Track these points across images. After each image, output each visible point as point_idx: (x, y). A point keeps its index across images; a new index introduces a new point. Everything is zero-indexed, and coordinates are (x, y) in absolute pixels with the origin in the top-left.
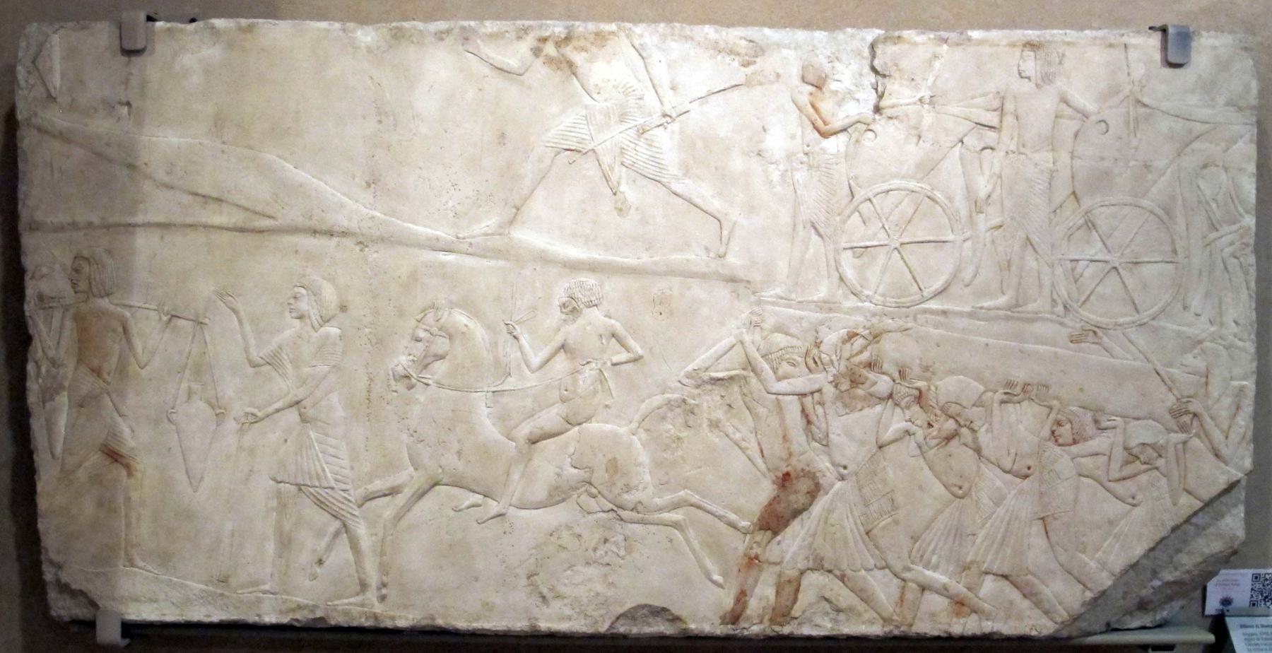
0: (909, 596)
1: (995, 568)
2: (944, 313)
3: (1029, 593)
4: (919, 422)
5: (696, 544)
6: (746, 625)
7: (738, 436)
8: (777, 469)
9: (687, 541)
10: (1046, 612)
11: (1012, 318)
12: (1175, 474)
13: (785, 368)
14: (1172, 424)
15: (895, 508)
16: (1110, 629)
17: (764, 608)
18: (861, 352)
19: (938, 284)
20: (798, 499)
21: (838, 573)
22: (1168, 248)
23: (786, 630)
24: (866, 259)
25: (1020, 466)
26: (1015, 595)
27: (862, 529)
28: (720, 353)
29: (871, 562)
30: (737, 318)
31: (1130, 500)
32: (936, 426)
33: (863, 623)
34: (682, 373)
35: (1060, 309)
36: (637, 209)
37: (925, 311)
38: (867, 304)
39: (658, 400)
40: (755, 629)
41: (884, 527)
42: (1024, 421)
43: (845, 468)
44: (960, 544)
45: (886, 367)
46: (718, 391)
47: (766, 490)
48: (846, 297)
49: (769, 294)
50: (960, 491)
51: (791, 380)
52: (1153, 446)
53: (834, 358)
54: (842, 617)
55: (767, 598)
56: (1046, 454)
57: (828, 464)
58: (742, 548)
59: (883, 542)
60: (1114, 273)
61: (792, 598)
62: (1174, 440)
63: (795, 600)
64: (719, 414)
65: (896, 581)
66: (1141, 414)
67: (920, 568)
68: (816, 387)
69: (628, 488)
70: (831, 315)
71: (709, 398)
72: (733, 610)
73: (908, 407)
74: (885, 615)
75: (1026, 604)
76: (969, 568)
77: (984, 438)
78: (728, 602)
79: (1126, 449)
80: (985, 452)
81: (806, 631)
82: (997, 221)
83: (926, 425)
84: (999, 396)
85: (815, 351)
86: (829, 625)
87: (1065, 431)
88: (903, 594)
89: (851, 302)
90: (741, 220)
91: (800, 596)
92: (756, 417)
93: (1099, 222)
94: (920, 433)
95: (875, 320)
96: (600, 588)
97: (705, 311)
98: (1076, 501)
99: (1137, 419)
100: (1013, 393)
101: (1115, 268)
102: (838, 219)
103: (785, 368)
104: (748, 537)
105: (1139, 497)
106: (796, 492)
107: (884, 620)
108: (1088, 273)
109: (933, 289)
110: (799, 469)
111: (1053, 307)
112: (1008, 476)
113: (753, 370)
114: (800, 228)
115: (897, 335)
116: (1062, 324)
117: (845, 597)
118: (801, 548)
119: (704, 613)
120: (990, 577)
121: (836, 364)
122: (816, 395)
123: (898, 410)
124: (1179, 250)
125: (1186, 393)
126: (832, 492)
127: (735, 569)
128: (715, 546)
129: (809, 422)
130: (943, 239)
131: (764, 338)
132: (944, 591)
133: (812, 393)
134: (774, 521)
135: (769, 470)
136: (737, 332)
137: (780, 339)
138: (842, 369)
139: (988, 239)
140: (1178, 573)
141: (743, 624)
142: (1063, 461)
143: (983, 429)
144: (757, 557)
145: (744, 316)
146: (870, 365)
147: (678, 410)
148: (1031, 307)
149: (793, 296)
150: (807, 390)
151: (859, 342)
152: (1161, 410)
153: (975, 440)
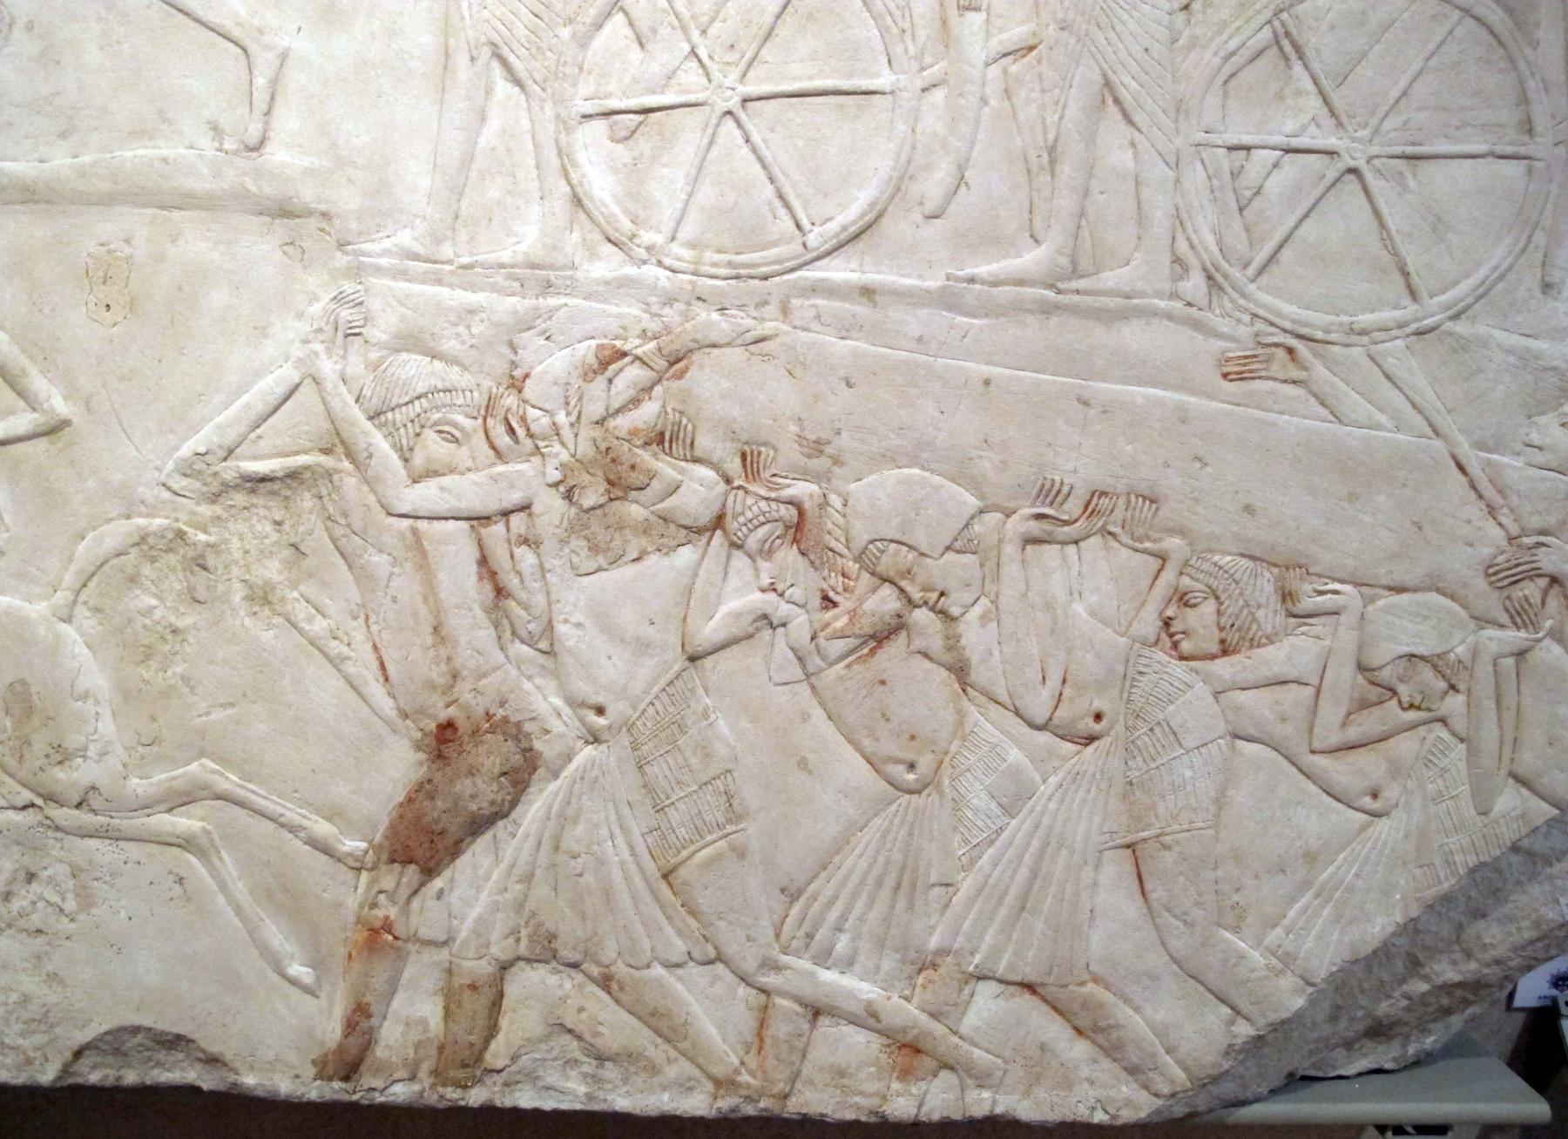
0: (779, 1029)
1: (1001, 969)
2: (868, 293)
3: (1091, 1026)
4: (796, 593)
5: (240, 888)
6: (378, 1083)
7: (319, 626)
8: (422, 712)
9: (224, 887)
10: (1132, 1071)
11: (1058, 308)
12: (1489, 735)
13: (433, 447)
14: (1492, 603)
15: (735, 816)
16: (1298, 1081)
17: (418, 1046)
18: (635, 402)
19: (850, 213)
20: (481, 791)
21: (595, 971)
22: (1508, 115)
23: (475, 1097)
24: (643, 144)
25: (1074, 711)
26: (1055, 1031)
27: (651, 866)
28: (260, 408)
29: (679, 947)
30: (300, 316)
31: (1367, 801)
32: (845, 603)
33: (664, 1088)
34: (170, 465)
35: (1194, 285)
36: (30, 27)
37: (814, 289)
38: (651, 271)
39: (114, 534)
40: (401, 1092)
41: (707, 865)
42: (1089, 595)
43: (600, 711)
44: (911, 907)
45: (704, 443)
46: (267, 507)
47: (398, 766)
48: (593, 254)
49: (379, 248)
50: (911, 774)
51: (446, 480)
52: (1434, 662)
53: (562, 418)
54: (610, 1072)
55: (423, 1022)
56: (1145, 683)
57: (557, 701)
58: (352, 902)
59: (705, 900)
60: (1352, 183)
61: (481, 1022)
62: (1494, 648)
63: (492, 1030)
64: (272, 570)
65: (742, 990)
66: (1409, 579)
67: (805, 964)
68: (515, 497)
69: (63, 755)
70: (552, 301)
71: (241, 527)
72: (341, 1049)
73: (767, 552)
74: (719, 1071)
75: (1080, 1050)
76: (934, 966)
77: (975, 636)
78: (331, 1031)
79: (1362, 668)
80: (978, 675)
81: (526, 1099)
82: (1016, 34)
83: (816, 602)
84: (1018, 524)
85: (510, 400)
86: (582, 1089)
87: (1201, 621)
88: (762, 1024)
89: (606, 265)
90: (301, 46)
91: (504, 1022)
92: (364, 577)
93: (1310, 41)
94: (801, 624)
95: (671, 314)
96: (29, 984)
97: (218, 297)
98: (1221, 801)
99: (1400, 589)
100: (1062, 516)
101: (1353, 171)
102: (565, 33)
103: (433, 447)
104: (365, 875)
105: (1392, 792)
106: (471, 773)
107: (718, 1083)
108: (1276, 185)
109: (833, 226)
110: (480, 711)
111: (1177, 279)
112: (1044, 738)
113: (350, 455)
114: (462, 60)
115: (737, 355)
116: (1197, 325)
117: (616, 1025)
118: (495, 908)
119: (276, 1053)
120: (986, 989)
121: (567, 434)
122: (517, 521)
123: (740, 561)
124: (1540, 123)
125: (1535, 522)
126: (570, 769)
127: (342, 951)
128: (287, 899)
129: (500, 592)
130: (865, 84)
131: (374, 367)
132: (868, 1018)
133: (506, 514)
134: (423, 843)
135: (405, 715)
136: (298, 351)
137: (416, 370)
138: (585, 449)
139: (993, 88)
140: (1473, 965)
141: (368, 1081)
142: (1188, 697)
143: (977, 611)
144: (387, 926)
145: (316, 308)
146: (659, 439)
147: (172, 559)
148: (1110, 278)
149: (447, 251)
150: (493, 505)
151: (632, 375)
152: (1463, 564)
153: (953, 642)
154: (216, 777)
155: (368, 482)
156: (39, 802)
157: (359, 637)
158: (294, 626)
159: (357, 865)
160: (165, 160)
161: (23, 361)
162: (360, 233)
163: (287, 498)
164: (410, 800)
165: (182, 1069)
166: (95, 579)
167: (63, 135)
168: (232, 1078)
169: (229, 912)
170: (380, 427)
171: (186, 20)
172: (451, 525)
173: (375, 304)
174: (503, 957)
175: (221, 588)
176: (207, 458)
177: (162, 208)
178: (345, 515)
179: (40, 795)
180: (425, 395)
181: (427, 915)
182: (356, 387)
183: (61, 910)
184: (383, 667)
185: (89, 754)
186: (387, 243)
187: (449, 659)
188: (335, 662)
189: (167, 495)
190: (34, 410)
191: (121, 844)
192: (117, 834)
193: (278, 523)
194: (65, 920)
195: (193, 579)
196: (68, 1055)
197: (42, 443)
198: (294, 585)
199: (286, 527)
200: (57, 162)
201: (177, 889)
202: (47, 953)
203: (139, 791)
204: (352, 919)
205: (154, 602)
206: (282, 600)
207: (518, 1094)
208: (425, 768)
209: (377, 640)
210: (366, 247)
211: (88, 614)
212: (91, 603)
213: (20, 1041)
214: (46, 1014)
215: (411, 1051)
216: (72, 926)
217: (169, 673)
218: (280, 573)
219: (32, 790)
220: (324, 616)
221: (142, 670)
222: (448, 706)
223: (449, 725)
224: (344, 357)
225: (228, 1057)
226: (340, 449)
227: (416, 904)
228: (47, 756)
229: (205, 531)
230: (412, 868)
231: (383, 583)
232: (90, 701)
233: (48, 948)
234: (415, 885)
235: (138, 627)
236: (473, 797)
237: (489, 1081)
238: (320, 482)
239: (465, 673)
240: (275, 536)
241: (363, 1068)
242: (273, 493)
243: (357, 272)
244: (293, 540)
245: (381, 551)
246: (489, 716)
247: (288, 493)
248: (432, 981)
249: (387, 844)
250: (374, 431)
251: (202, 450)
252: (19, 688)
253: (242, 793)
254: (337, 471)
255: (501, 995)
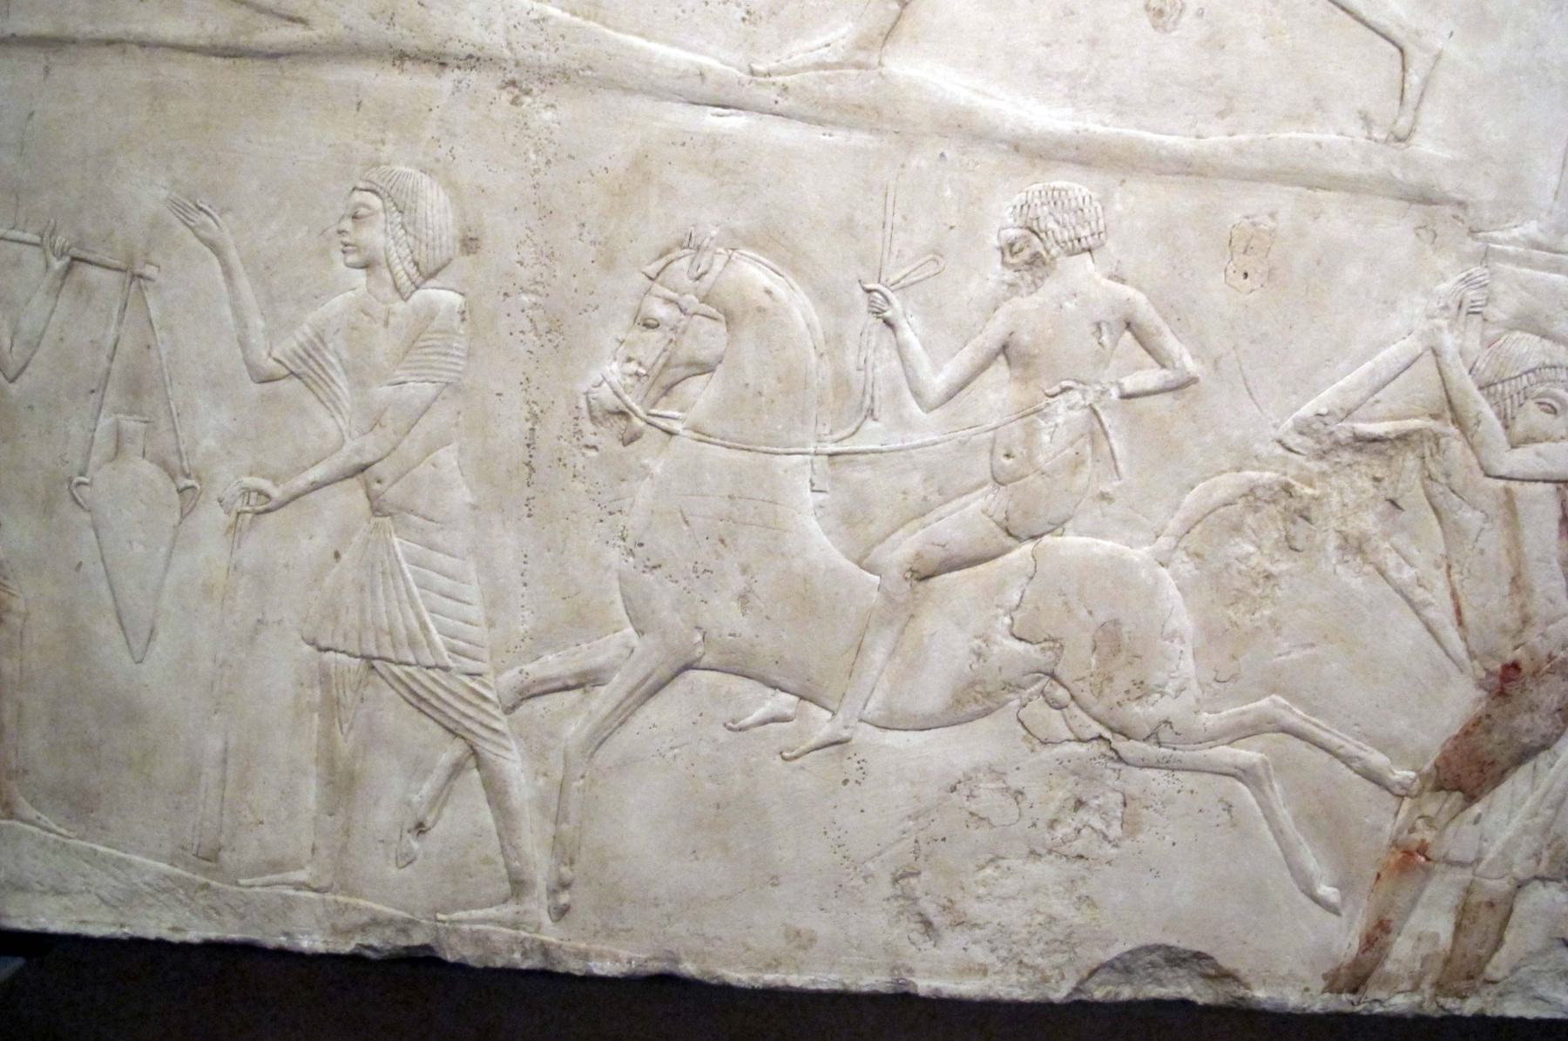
5: (1284, 814)
6: (1382, 995)
7: (1407, 574)
8: (1491, 654)
13: (1533, 417)
17: (1425, 960)
23: (1470, 1007)
34: (1289, 422)
36: (1200, 13)
39: (1226, 484)
40: (1400, 1003)
47: (1461, 699)
49: (1513, 234)
51: (1541, 447)
58: (1389, 828)
64: (1368, 522)
69: (1141, 690)
71: (1343, 483)
72: (1356, 963)
81: (1513, 1008)
90: (1454, 51)
91: (1509, 936)
96: (1059, 907)
97: (1353, 273)
103: (1533, 417)
106: (1532, 708)
113: (1457, 420)
118: (1525, 830)
127: (1372, 872)
135: (1472, 655)
137: (1528, 348)
141: (1373, 992)
144: (1423, 849)
147: (1272, 510)
154: (1283, 712)
155: (1472, 448)
156: (1107, 735)
157: (1440, 584)
158: (1382, 573)
159: (1403, 792)
160: (1319, 145)
161: (1159, 321)
162: (1492, 222)
163: (1391, 457)
164: (1466, 733)
165: (1179, 984)
166: (1199, 527)
167: (1221, 115)
168: (1241, 992)
169: (1270, 837)
170: (1488, 396)
171: (1348, 18)
172: (1540, 487)
173: (1500, 287)
174: (1522, 875)
175: (1319, 538)
176: (1327, 419)
177: (1309, 187)
178: (1448, 475)
179: (1111, 729)
180: (1533, 371)
181: (1460, 838)
182: (1471, 360)
183: (1105, 837)
184: (1458, 612)
185: (1167, 689)
186: (1516, 232)
187: (1523, 606)
188: (1416, 608)
189: (1280, 451)
190: (1163, 366)
191: (1178, 774)
192: (1176, 765)
193: (1376, 479)
194: (1107, 846)
195: (1293, 529)
196: (1085, 974)
197: (1166, 399)
198: (1387, 536)
199: (1386, 483)
200: (1213, 139)
201: (1226, 816)
202: (1083, 878)
203: (1209, 724)
204: (1386, 842)
205: (1252, 549)
206: (1376, 550)
207: (1506, 1004)
208: (1484, 704)
209: (1458, 587)
210: (1495, 234)
211: (1186, 559)
212: (1191, 550)
213: (1039, 961)
214: (1069, 936)
215: (1418, 965)
216: (1114, 851)
217: (1257, 615)
218: (1375, 525)
219: (1101, 722)
220: (1412, 566)
221: (1230, 612)
222: (1516, 648)
223: (1515, 666)
224: (1463, 333)
225: (1243, 970)
226: (1448, 415)
227: (1450, 830)
228: (1127, 692)
229: (1311, 485)
230: (1458, 794)
231: (1473, 537)
232: (1176, 640)
233: (1086, 873)
234: (1455, 810)
235: (1234, 572)
236: (1528, 731)
237: (1484, 992)
238: (1426, 444)
239: (1536, 619)
240: (1372, 491)
241: (1370, 982)
242: (1381, 453)
243: (1486, 256)
244: (1391, 495)
245: (1475, 508)
246: (1551, 657)
247: (1392, 452)
248: (1451, 898)
249: (1434, 773)
250: (1482, 400)
251: (1324, 410)
252: (1110, 627)
253: (1308, 727)
254: (1445, 435)
255: (1511, 911)
